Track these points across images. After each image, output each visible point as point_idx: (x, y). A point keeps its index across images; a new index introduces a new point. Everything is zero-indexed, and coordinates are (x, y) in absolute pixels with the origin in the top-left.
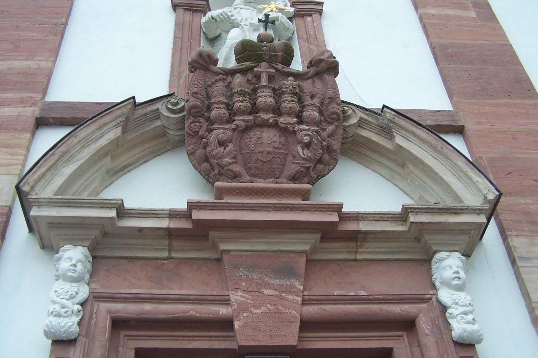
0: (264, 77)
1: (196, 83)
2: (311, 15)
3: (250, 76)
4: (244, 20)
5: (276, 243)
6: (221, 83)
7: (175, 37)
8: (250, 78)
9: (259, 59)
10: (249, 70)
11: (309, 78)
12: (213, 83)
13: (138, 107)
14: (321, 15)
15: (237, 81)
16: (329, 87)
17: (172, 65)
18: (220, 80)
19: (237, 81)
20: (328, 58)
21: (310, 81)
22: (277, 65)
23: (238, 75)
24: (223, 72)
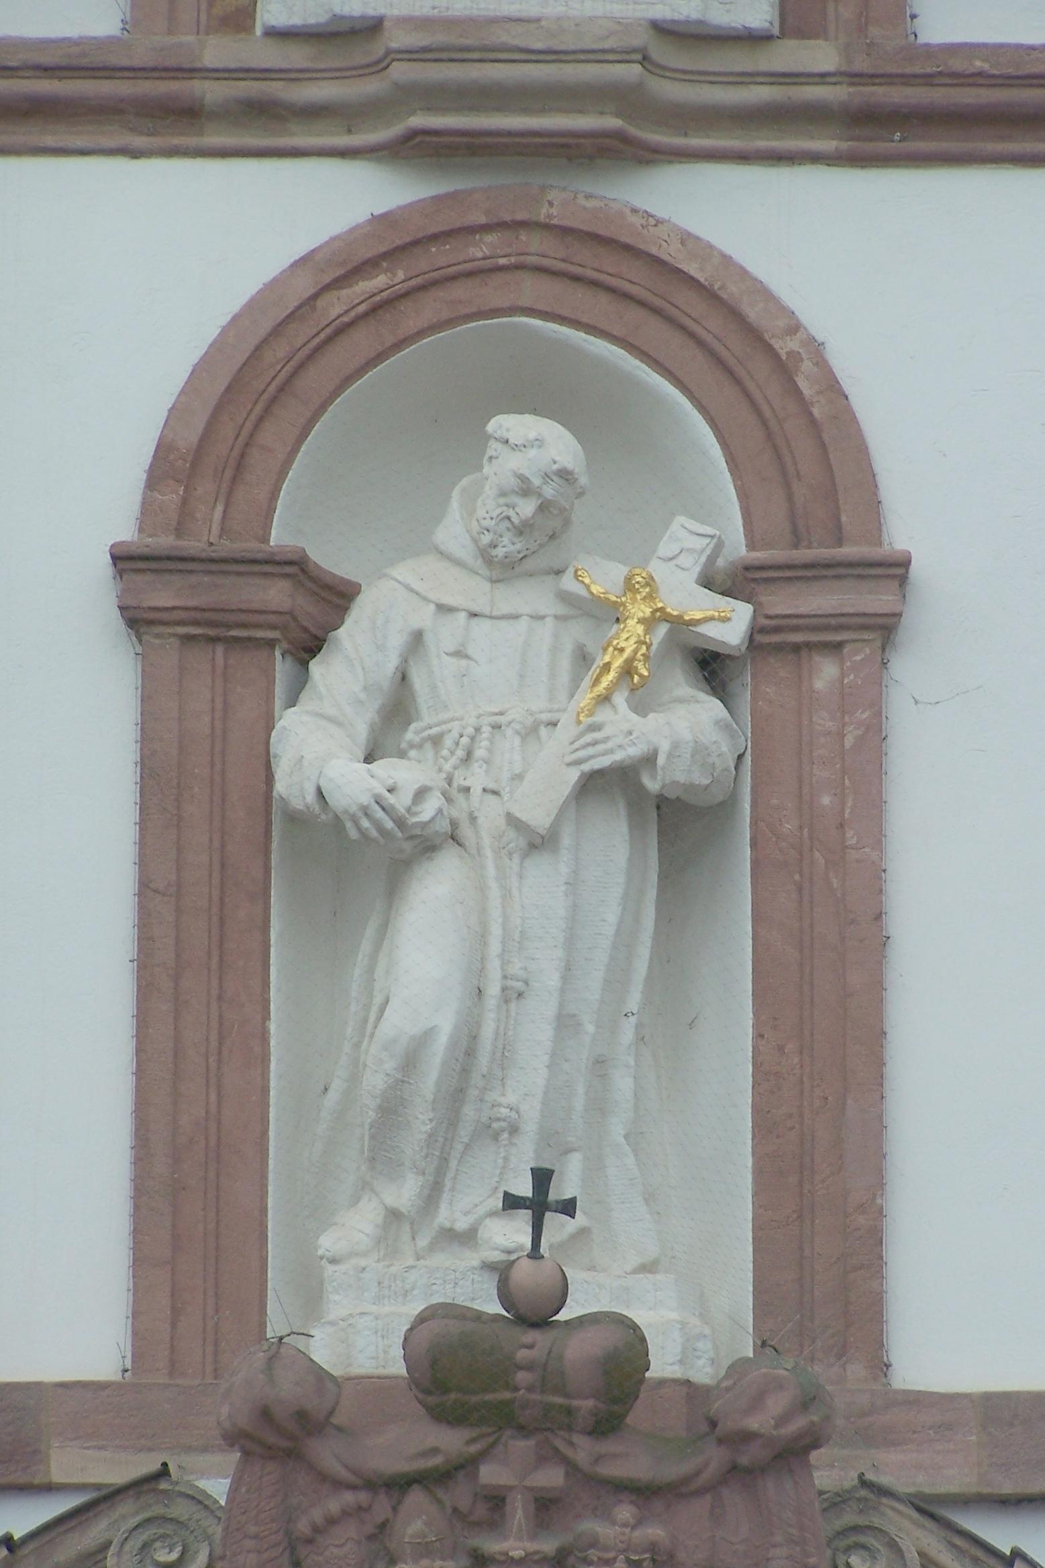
0: (519, 1514)
1: (253, 1529)
2: (836, 648)
3: (460, 1495)
4: (486, 730)
5: (870, 140)
6: (350, 1531)
7: (145, 888)
8: (464, 1504)
9: (505, 1419)
10: (460, 1467)
11: (699, 1492)
12: (316, 1530)
13: (26, 1550)
14: (903, 580)
15: (410, 1530)
16: (778, 1539)
17: (139, 1027)
18: (346, 1513)
19: (410, 1530)
20: (776, 1426)
21: (701, 1506)
22: (571, 1444)
23: (416, 1497)
24: (358, 1482)
